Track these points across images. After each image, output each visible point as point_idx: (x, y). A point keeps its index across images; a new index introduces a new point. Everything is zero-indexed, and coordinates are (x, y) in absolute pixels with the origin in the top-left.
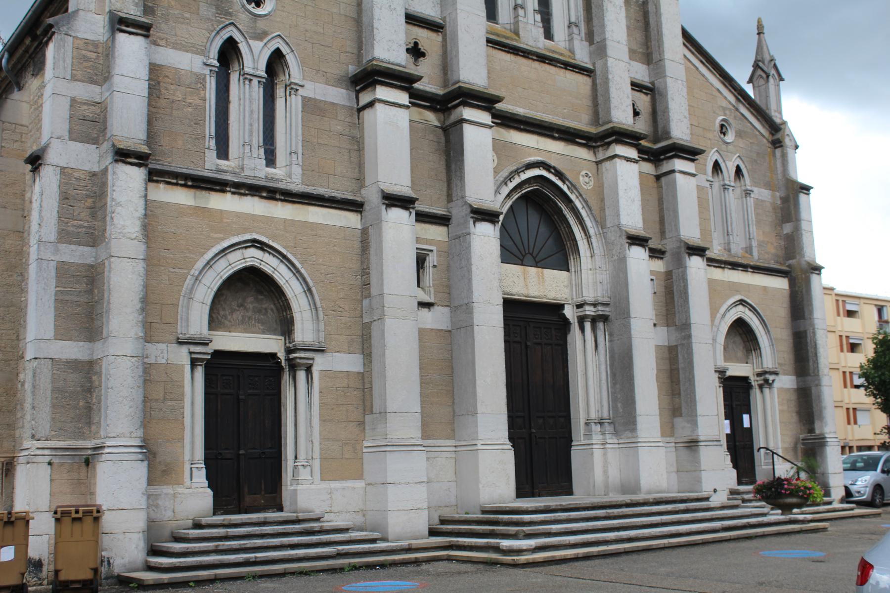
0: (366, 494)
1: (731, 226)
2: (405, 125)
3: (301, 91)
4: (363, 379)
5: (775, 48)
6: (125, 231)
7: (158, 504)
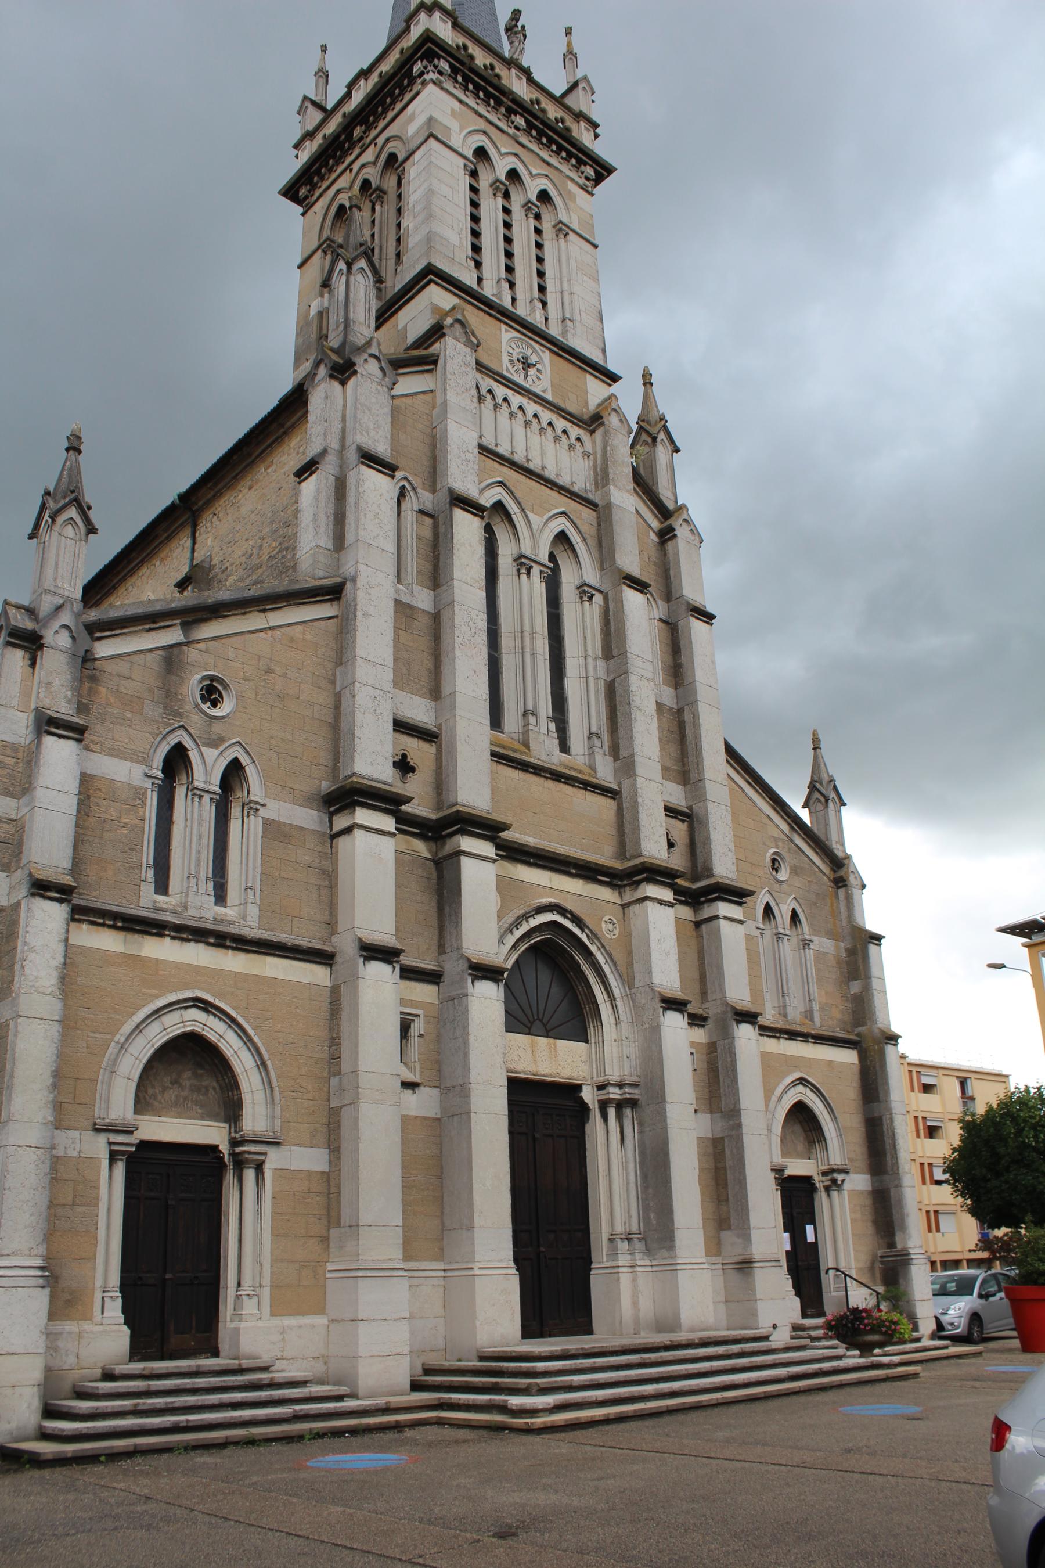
0: (328, 1335)
1: (787, 984)
2: (390, 857)
3: (262, 812)
4: (328, 1180)
5: (835, 768)
6: (37, 984)
7: (58, 1346)
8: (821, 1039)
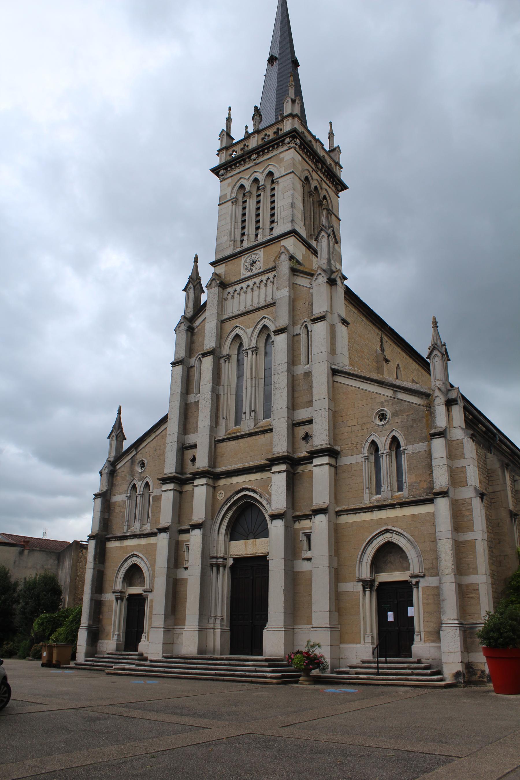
8: (403, 504)
